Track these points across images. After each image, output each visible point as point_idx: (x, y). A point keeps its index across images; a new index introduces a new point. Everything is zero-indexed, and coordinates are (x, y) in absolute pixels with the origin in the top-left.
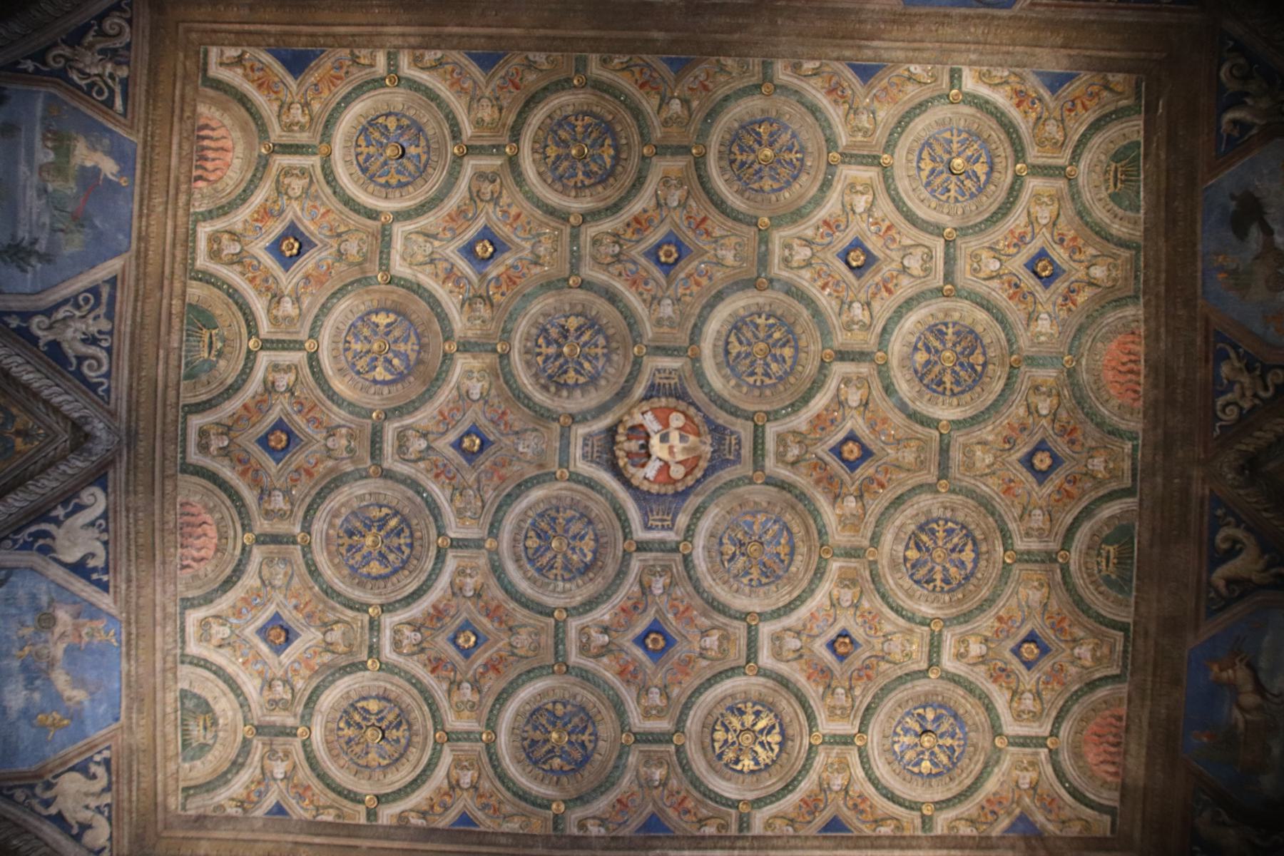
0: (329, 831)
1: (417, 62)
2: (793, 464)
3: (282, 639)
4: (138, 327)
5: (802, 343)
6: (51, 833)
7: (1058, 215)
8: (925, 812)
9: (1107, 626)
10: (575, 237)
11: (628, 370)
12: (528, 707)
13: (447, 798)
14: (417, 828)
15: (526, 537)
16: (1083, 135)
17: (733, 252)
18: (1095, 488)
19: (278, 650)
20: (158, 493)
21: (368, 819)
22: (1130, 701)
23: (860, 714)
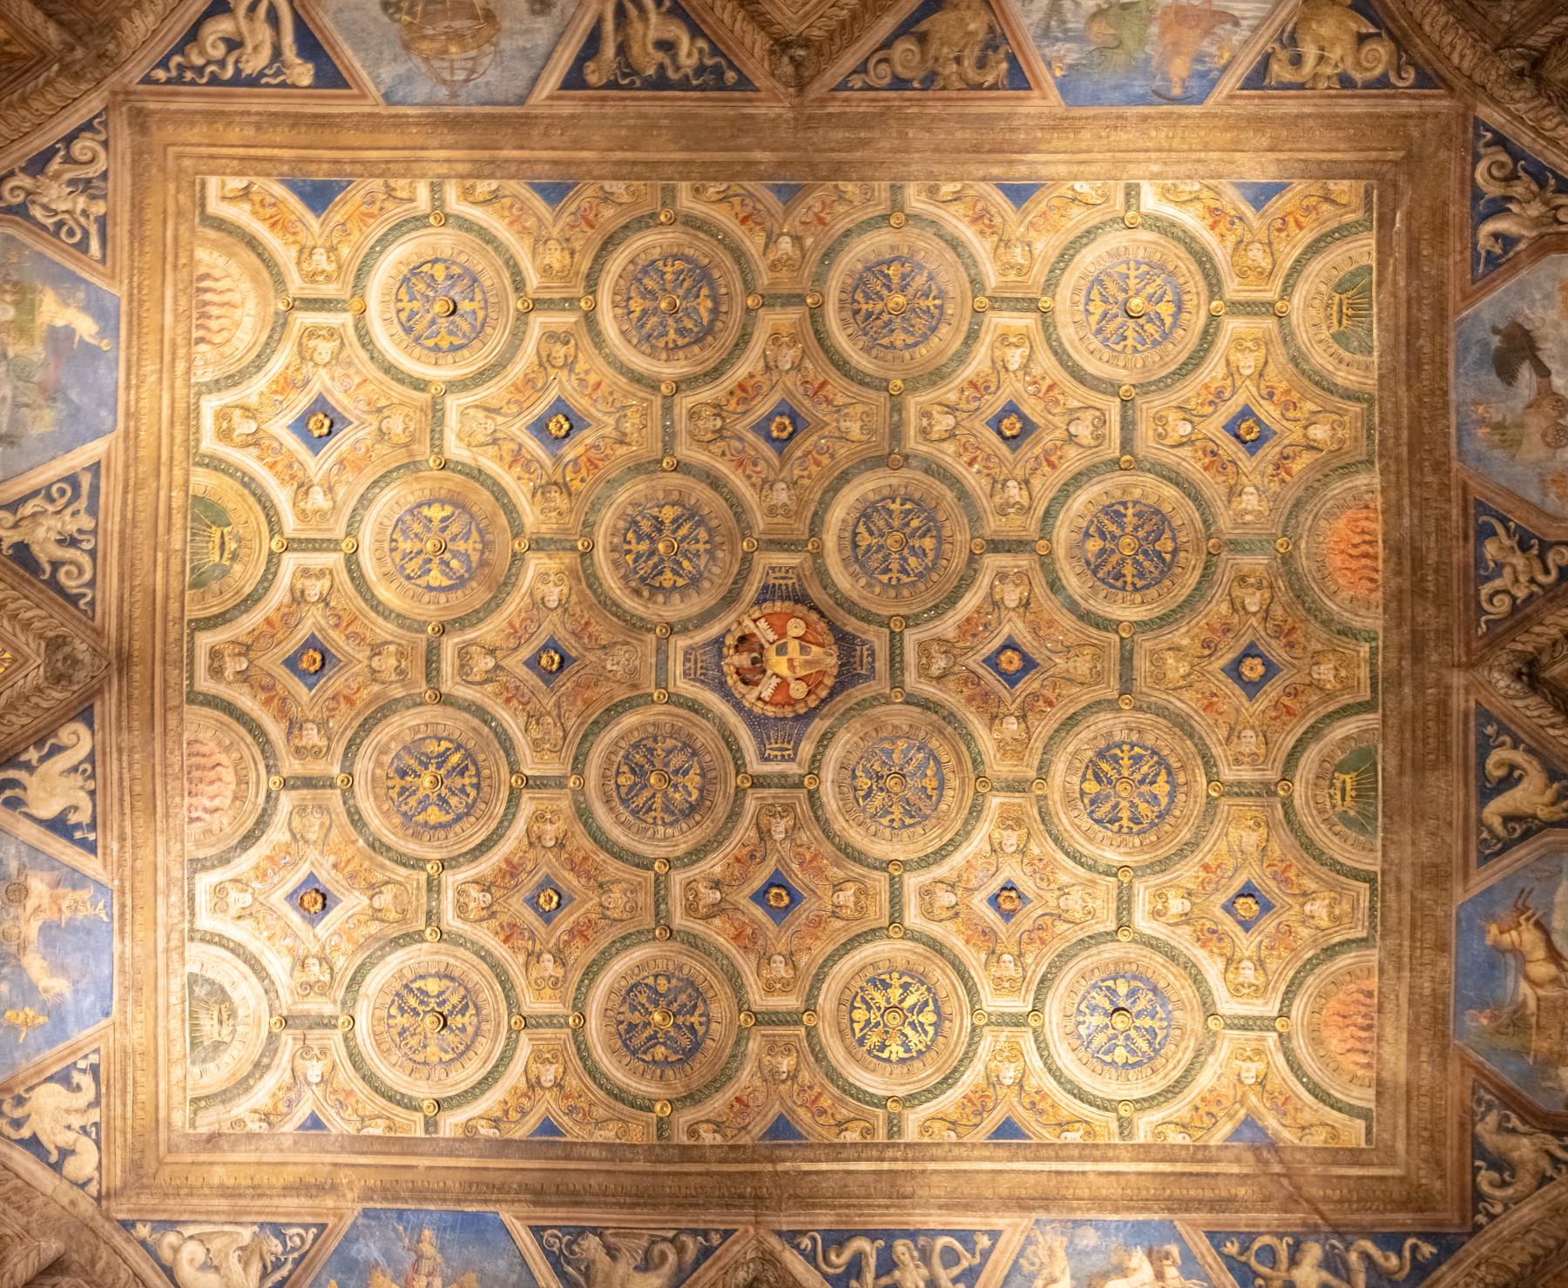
0: (376, 1147)
1: (467, 193)
2: (939, 678)
3: (319, 906)
4: (129, 524)
5: (946, 532)
6: (23, 1161)
7: (1266, 363)
8: (1122, 1113)
9: (1346, 876)
10: (668, 410)
11: (735, 570)
12: (623, 983)
13: (524, 1101)
14: (488, 1140)
15: (618, 773)
16: (1298, 261)
17: (859, 424)
18: (1322, 702)
19: (313, 920)
20: (158, 729)
21: (427, 1131)
22: (1382, 971)
23: (1034, 987)
